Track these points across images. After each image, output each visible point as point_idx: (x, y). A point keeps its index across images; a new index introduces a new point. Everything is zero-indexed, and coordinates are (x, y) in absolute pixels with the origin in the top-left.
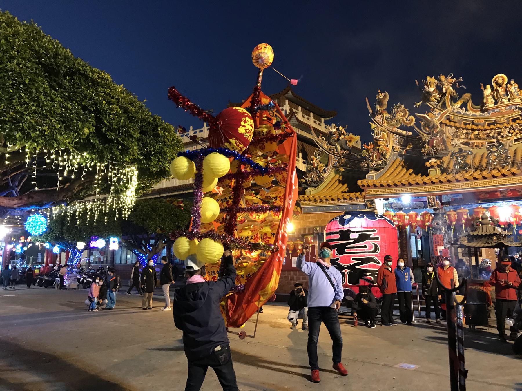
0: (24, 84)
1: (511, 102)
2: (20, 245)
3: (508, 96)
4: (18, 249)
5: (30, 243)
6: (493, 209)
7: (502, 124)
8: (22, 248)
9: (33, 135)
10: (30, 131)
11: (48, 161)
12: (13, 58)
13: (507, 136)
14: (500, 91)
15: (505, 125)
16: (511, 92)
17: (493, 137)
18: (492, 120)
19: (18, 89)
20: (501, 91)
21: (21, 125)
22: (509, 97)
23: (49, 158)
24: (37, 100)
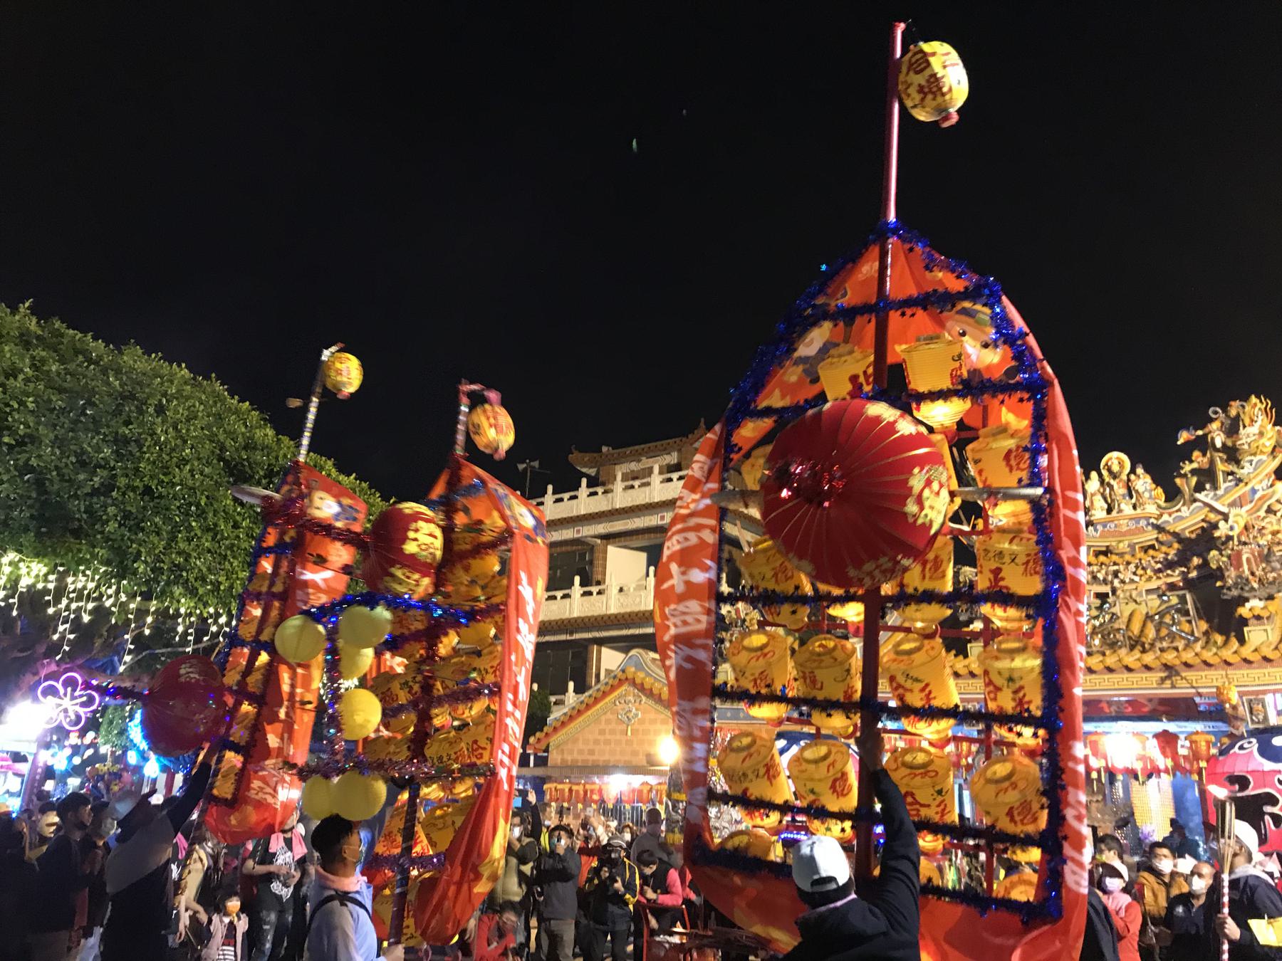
0: (198, 505)
1: (1139, 511)
2: (68, 751)
3: (1131, 497)
4: (60, 764)
5: (88, 747)
6: (1093, 738)
7: (1121, 555)
8: (70, 758)
9: (201, 591)
10: (197, 584)
11: (214, 629)
12: (185, 461)
13: (1132, 581)
14: (1116, 487)
15: (1128, 557)
16: (1137, 492)
17: (1105, 582)
18: (1102, 544)
19: (187, 514)
20: (1120, 490)
21: (184, 574)
22: (1134, 501)
23: (216, 622)
24: (213, 530)
